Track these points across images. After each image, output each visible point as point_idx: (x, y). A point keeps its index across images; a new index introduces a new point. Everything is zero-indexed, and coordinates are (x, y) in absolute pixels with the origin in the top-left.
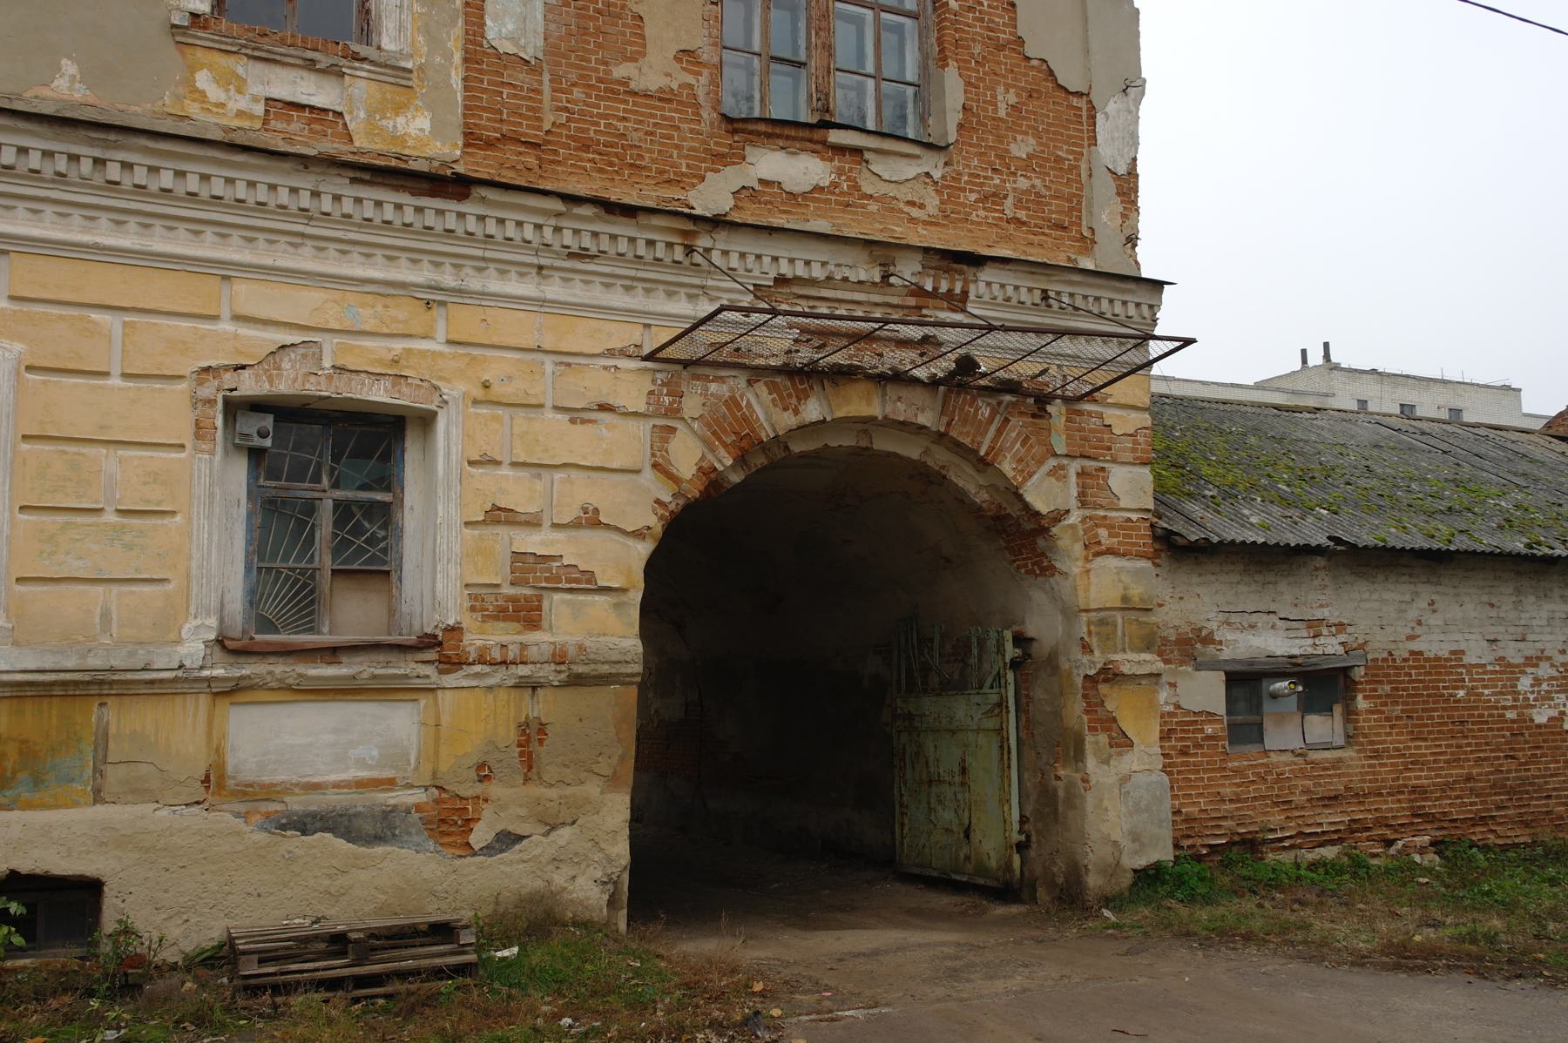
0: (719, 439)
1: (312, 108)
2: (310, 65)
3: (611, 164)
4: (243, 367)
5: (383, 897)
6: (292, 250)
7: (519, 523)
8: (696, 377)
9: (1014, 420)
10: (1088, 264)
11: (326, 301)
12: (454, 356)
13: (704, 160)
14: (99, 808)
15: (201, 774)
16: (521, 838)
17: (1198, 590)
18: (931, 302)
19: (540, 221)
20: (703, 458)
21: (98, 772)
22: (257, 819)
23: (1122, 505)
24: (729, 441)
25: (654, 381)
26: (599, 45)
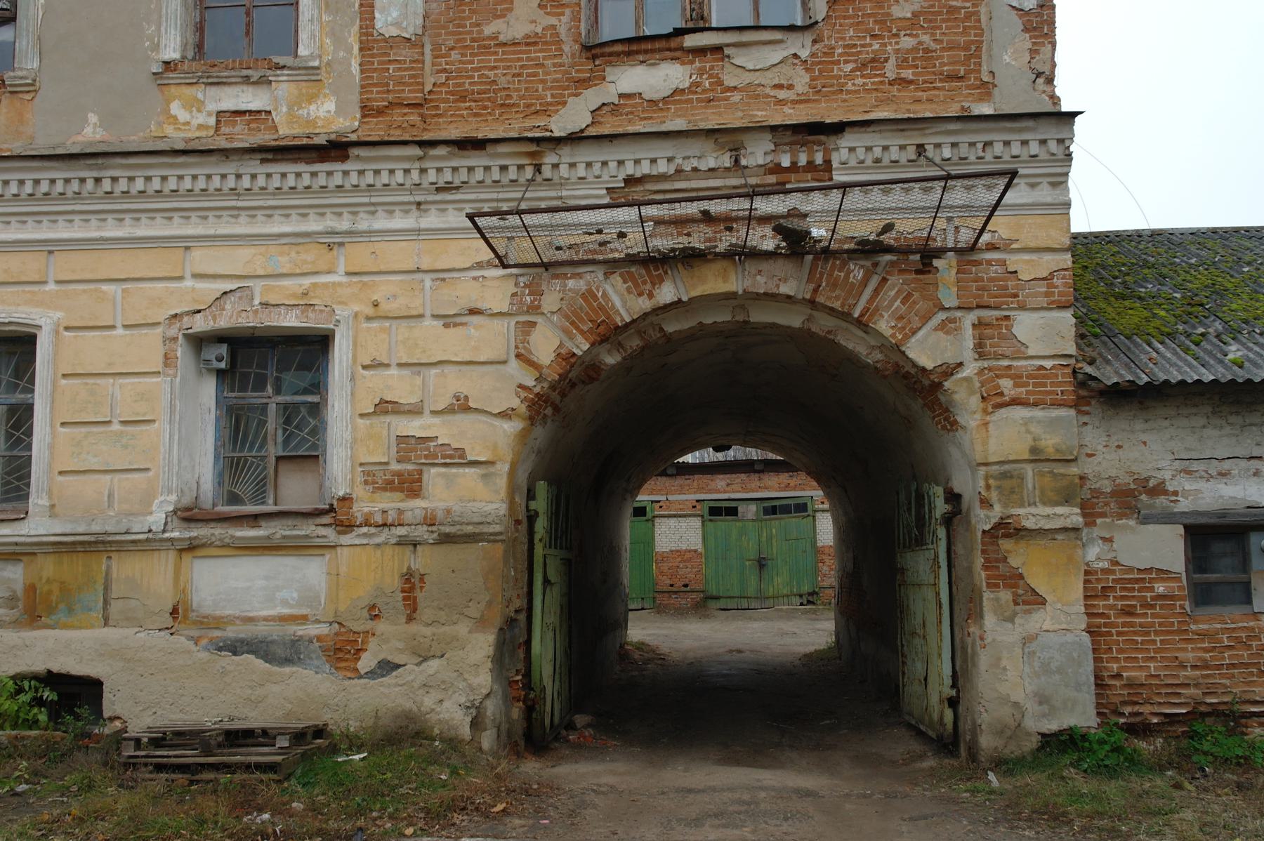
0: (577, 328)
1: (250, 112)
2: (247, 80)
3: (485, 108)
4: (199, 311)
5: (290, 706)
6: (233, 220)
7: (404, 413)
8: (556, 276)
9: (892, 279)
10: (987, 110)
11: (254, 255)
12: (350, 284)
13: (567, 88)
14: (106, 629)
15: (169, 608)
16: (398, 666)
17: (1144, 437)
18: (793, 177)
19: (407, 166)
20: (561, 345)
21: (106, 602)
22: (204, 642)
23: (1031, 352)
24: (585, 328)
25: (516, 284)
26: (473, 12)
